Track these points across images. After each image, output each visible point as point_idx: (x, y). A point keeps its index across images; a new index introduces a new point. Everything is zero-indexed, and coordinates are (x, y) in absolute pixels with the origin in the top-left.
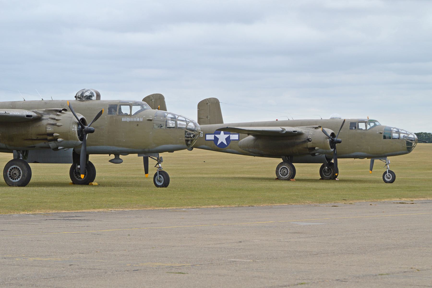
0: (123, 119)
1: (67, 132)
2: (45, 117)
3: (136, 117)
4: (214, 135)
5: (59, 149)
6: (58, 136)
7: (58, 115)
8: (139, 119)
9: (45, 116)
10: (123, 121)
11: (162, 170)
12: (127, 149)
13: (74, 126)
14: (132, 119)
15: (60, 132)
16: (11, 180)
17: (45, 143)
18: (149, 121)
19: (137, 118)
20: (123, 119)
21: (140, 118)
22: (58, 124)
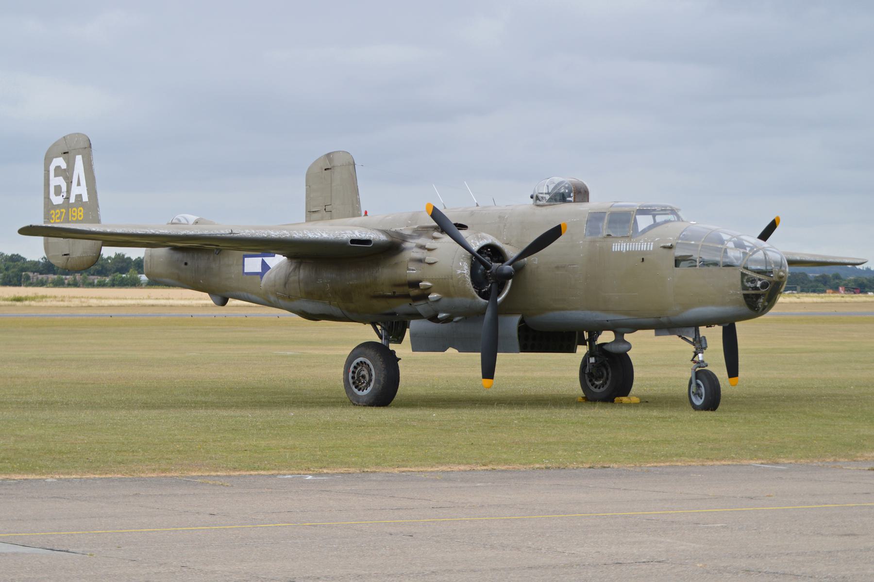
0: (613, 247)
1: (444, 277)
2: (410, 244)
3: (641, 240)
4: (260, 259)
5: (441, 318)
6: (429, 288)
7: (435, 238)
8: (645, 246)
9: (411, 241)
10: (613, 250)
11: (706, 368)
12: (626, 317)
13: (463, 264)
14: (632, 245)
15: (432, 279)
16: (356, 390)
17: (410, 304)
18: (666, 250)
19: (641, 243)
20: (615, 245)
21: (649, 243)
22: (430, 257)
